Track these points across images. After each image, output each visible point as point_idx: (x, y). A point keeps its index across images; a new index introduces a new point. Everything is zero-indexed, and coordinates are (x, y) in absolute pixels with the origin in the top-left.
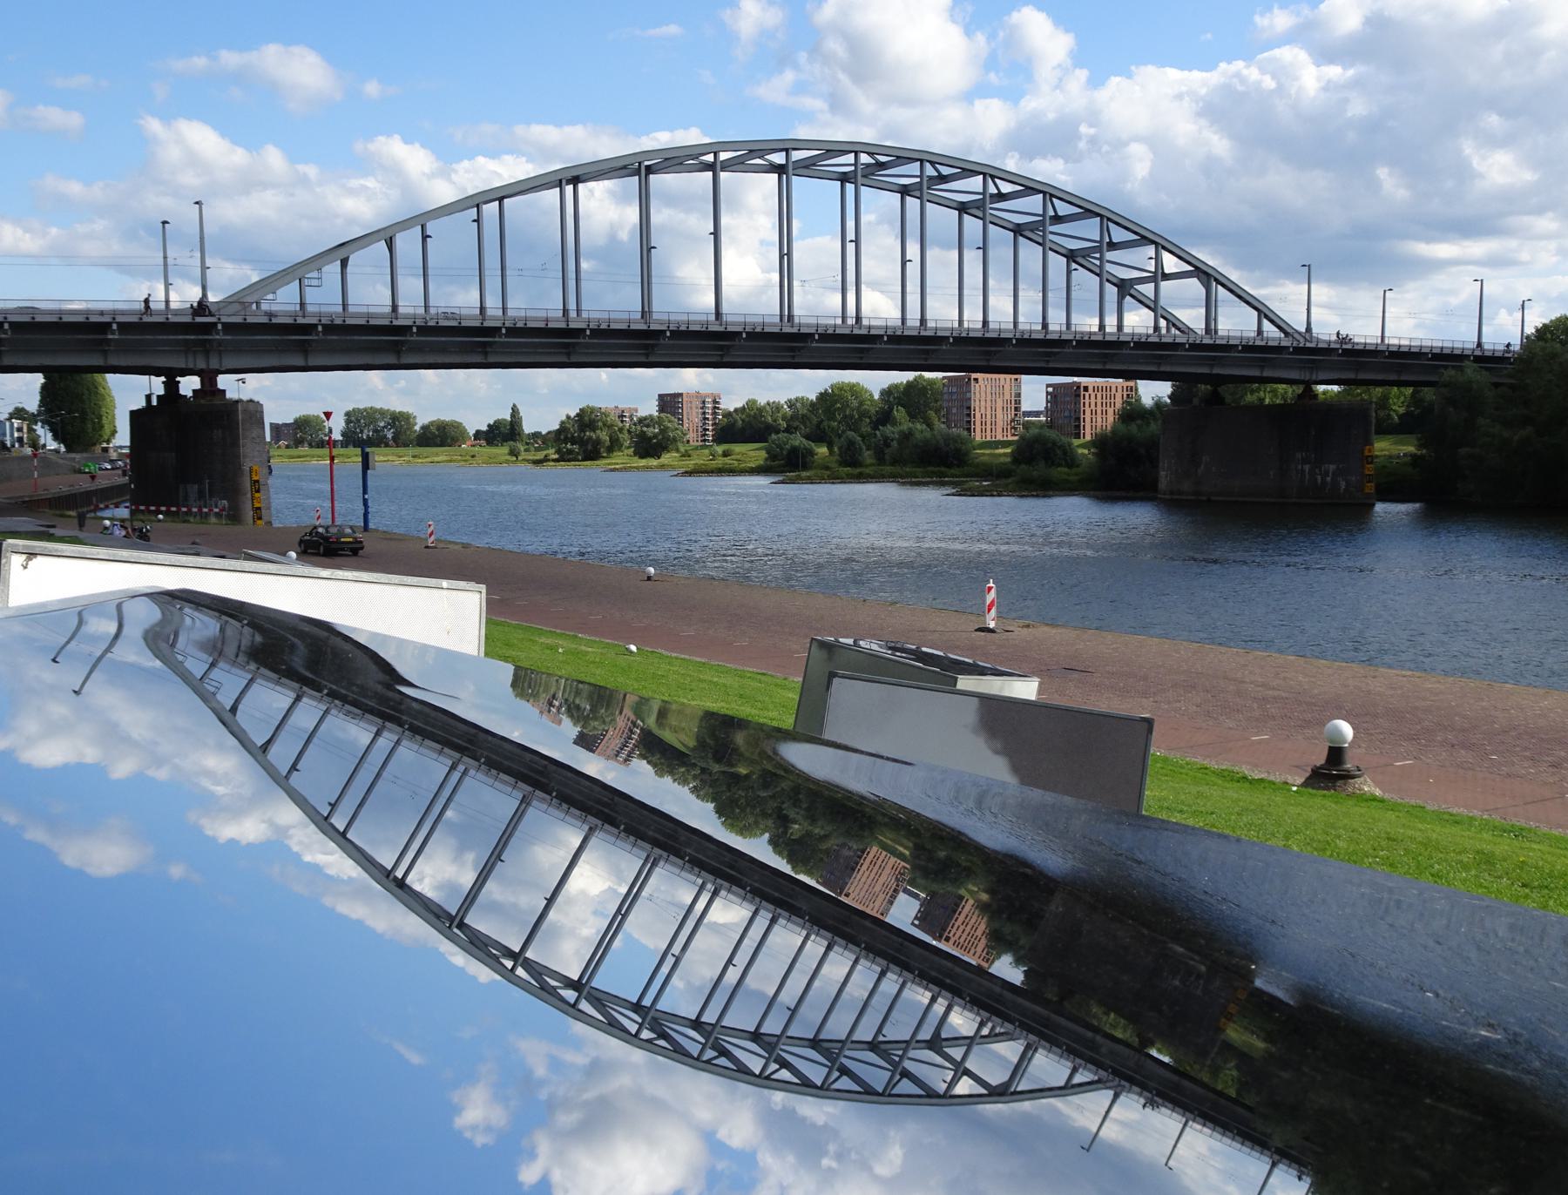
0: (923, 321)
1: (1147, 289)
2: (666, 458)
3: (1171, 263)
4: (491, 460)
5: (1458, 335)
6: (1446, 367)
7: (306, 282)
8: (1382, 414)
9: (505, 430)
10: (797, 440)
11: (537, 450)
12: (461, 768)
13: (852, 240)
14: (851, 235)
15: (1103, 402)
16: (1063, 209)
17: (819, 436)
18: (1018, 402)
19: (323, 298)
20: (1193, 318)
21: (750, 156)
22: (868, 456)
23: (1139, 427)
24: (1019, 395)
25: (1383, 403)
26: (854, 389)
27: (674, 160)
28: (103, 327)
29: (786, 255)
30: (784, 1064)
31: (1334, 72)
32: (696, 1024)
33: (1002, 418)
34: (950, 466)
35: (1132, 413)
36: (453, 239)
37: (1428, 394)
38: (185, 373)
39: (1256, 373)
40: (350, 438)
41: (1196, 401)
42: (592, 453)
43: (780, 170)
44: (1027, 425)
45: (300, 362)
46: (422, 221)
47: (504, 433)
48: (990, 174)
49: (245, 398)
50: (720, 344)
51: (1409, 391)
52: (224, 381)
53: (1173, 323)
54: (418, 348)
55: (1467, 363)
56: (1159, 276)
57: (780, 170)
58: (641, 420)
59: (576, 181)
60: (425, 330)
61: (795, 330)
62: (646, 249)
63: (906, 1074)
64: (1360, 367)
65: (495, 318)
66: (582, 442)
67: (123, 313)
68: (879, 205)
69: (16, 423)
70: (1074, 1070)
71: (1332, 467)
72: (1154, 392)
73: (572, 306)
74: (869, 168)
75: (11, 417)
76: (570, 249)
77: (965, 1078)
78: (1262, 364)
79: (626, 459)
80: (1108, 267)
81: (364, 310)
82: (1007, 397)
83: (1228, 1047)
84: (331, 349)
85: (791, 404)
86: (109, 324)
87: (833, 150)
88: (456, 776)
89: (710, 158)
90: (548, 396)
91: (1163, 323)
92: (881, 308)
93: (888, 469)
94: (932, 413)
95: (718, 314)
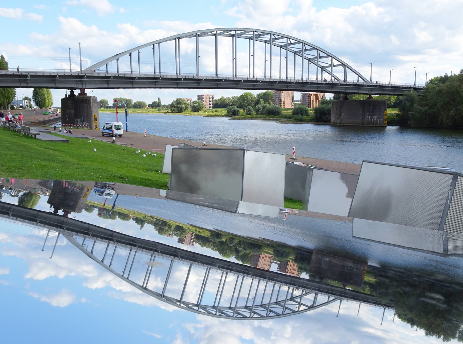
0: (270, 77)
1: (329, 69)
2: (200, 112)
3: (336, 62)
4: (153, 112)
5: (409, 82)
6: (405, 91)
7: (108, 65)
8: (389, 102)
9: (156, 104)
10: (235, 108)
11: (165, 109)
12: (154, 255)
13: (251, 55)
14: (252, 54)
15: (315, 100)
16: (308, 47)
17: (241, 106)
18: (293, 98)
19: (112, 70)
20: (341, 77)
21: (225, 32)
22: (254, 113)
23: (326, 106)
24: (293, 96)
25: (389, 100)
26: (250, 95)
27: (205, 33)
28: (55, 76)
29: (234, 59)
30: (255, 313)
31: (381, 9)
32: (230, 308)
33: (289, 102)
34: (275, 115)
35: (324, 102)
36: (147, 53)
37: (401, 97)
38: (75, 89)
39: (357, 92)
40: (115, 106)
41: (341, 99)
42: (180, 111)
43: (233, 36)
44: (295, 105)
45: (107, 86)
46: (138, 49)
47: (156, 105)
48: (288, 38)
49: (92, 96)
50: (217, 83)
51: (396, 96)
52: (87, 91)
53: (335, 78)
54: (137, 83)
55: (411, 89)
56: (333, 65)
57: (233, 36)
58: (193, 102)
59: (179, 38)
60: (139, 78)
61: (237, 79)
62: (198, 57)
63: (286, 308)
64: (383, 90)
65: (158, 75)
66: (177, 108)
67: (60, 73)
68: (259, 45)
69: (26, 101)
70: (329, 297)
71: (376, 117)
72: (329, 96)
73: (178, 72)
74: (256, 36)
75: (24, 99)
76: (178, 55)
77: (302, 306)
78: (359, 89)
79: (189, 112)
80: (319, 63)
81: (124, 72)
82: (290, 97)
83: (366, 283)
84: (115, 83)
85: (233, 98)
86: (56, 76)
87: (247, 31)
88: (153, 257)
89: (215, 33)
90: (168, 96)
91: (333, 78)
92: (259, 74)
93: (260, 116)
94: (270, 101)
95: (217, 75)
